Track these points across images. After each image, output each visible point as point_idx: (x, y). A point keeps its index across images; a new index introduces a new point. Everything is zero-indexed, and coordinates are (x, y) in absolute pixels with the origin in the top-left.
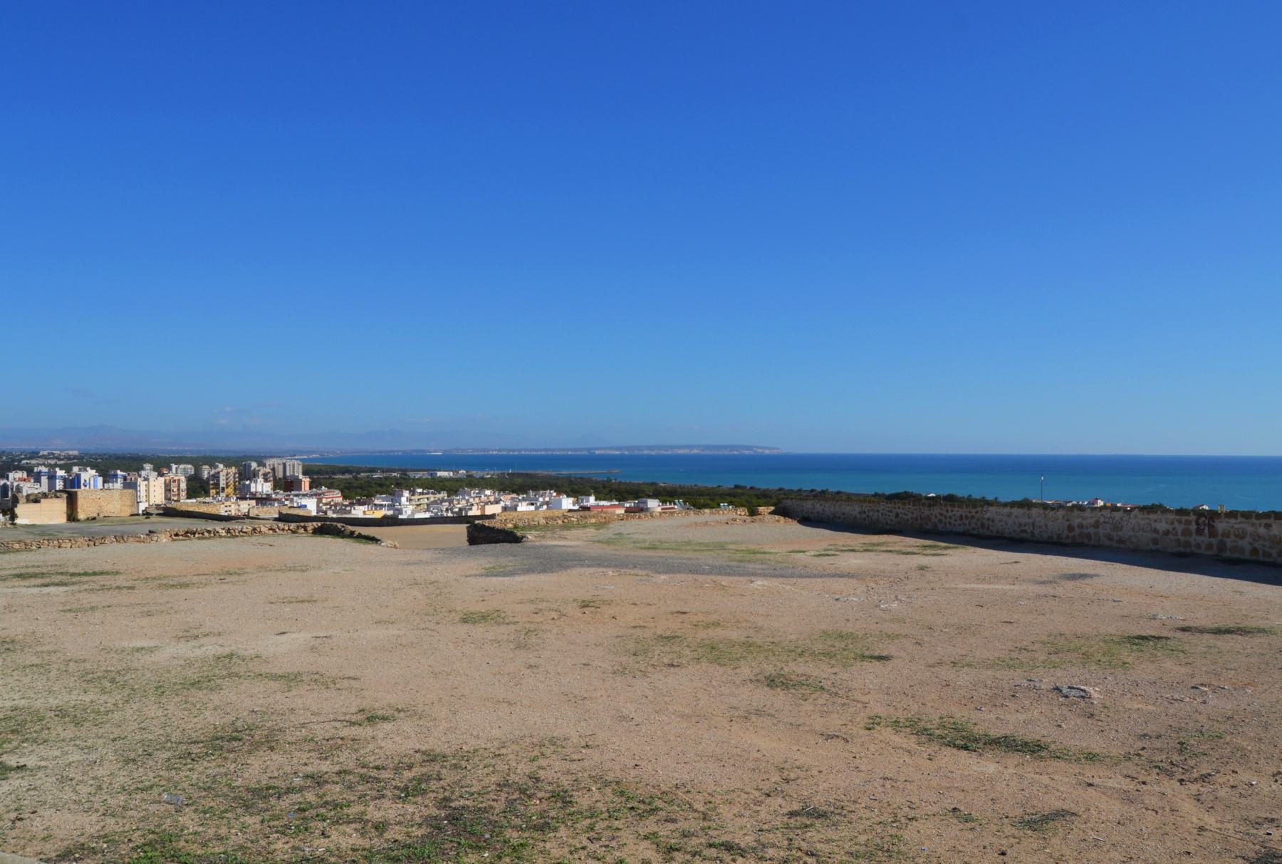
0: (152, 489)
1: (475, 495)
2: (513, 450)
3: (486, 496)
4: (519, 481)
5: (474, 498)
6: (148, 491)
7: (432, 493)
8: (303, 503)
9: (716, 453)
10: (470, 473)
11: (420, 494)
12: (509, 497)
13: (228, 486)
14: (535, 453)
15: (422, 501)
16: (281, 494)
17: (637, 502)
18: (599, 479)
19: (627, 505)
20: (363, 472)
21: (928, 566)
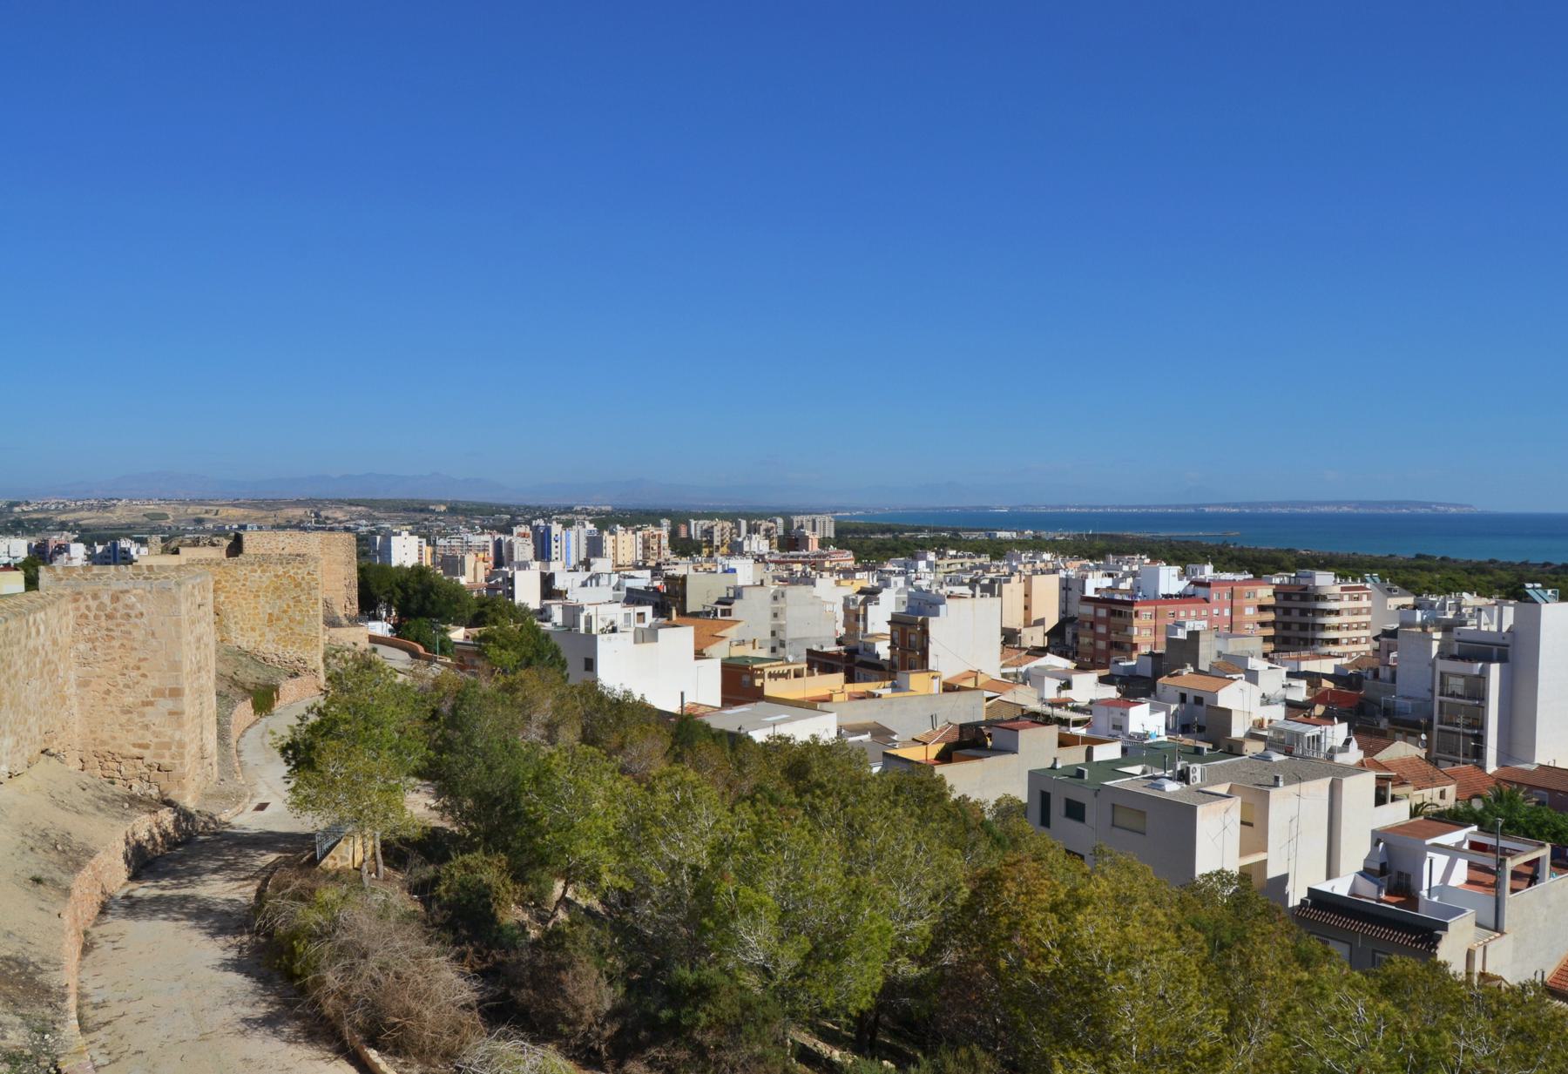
0: (620, 546)
1: (1027, 560)
2: (1097, 507)
3: (1043, 561)
4: (1100, 544)
5: (1025, 565)
6: (615, 548)
7: (970, 557)
8: (731, 566)
9: (1376, 511)
10: (1038, 534)
11: (955, 557)
12: (1077, 564)
13: (723, 545)
14: (1125, 511)
15: (953, 568)
16: (777, 555)
17: (1293, 575)
18: (1210, 544)
19: (1277, 580)
20: (907, 531)
21: (983, 801)
